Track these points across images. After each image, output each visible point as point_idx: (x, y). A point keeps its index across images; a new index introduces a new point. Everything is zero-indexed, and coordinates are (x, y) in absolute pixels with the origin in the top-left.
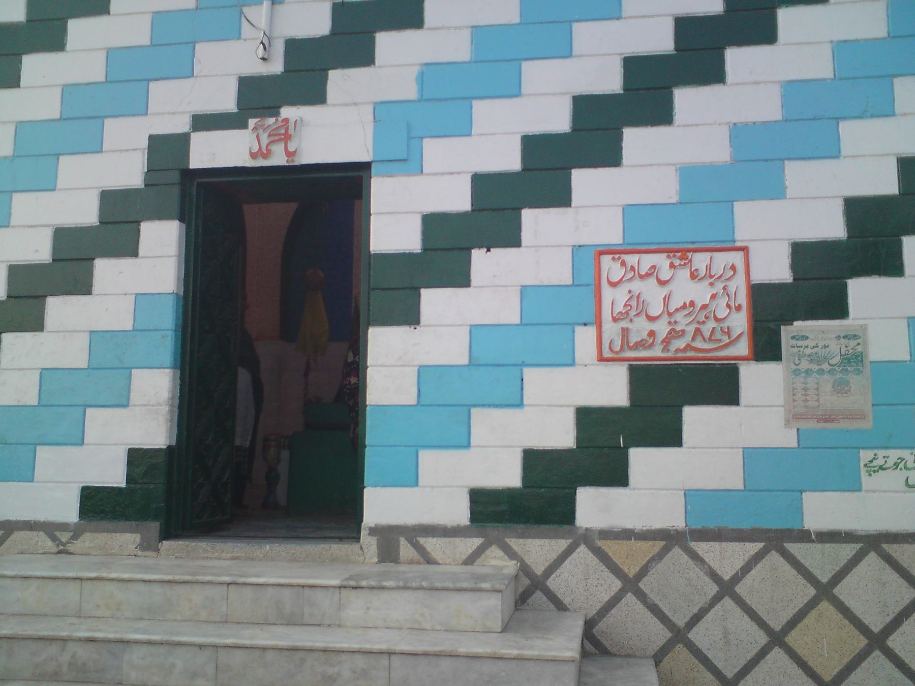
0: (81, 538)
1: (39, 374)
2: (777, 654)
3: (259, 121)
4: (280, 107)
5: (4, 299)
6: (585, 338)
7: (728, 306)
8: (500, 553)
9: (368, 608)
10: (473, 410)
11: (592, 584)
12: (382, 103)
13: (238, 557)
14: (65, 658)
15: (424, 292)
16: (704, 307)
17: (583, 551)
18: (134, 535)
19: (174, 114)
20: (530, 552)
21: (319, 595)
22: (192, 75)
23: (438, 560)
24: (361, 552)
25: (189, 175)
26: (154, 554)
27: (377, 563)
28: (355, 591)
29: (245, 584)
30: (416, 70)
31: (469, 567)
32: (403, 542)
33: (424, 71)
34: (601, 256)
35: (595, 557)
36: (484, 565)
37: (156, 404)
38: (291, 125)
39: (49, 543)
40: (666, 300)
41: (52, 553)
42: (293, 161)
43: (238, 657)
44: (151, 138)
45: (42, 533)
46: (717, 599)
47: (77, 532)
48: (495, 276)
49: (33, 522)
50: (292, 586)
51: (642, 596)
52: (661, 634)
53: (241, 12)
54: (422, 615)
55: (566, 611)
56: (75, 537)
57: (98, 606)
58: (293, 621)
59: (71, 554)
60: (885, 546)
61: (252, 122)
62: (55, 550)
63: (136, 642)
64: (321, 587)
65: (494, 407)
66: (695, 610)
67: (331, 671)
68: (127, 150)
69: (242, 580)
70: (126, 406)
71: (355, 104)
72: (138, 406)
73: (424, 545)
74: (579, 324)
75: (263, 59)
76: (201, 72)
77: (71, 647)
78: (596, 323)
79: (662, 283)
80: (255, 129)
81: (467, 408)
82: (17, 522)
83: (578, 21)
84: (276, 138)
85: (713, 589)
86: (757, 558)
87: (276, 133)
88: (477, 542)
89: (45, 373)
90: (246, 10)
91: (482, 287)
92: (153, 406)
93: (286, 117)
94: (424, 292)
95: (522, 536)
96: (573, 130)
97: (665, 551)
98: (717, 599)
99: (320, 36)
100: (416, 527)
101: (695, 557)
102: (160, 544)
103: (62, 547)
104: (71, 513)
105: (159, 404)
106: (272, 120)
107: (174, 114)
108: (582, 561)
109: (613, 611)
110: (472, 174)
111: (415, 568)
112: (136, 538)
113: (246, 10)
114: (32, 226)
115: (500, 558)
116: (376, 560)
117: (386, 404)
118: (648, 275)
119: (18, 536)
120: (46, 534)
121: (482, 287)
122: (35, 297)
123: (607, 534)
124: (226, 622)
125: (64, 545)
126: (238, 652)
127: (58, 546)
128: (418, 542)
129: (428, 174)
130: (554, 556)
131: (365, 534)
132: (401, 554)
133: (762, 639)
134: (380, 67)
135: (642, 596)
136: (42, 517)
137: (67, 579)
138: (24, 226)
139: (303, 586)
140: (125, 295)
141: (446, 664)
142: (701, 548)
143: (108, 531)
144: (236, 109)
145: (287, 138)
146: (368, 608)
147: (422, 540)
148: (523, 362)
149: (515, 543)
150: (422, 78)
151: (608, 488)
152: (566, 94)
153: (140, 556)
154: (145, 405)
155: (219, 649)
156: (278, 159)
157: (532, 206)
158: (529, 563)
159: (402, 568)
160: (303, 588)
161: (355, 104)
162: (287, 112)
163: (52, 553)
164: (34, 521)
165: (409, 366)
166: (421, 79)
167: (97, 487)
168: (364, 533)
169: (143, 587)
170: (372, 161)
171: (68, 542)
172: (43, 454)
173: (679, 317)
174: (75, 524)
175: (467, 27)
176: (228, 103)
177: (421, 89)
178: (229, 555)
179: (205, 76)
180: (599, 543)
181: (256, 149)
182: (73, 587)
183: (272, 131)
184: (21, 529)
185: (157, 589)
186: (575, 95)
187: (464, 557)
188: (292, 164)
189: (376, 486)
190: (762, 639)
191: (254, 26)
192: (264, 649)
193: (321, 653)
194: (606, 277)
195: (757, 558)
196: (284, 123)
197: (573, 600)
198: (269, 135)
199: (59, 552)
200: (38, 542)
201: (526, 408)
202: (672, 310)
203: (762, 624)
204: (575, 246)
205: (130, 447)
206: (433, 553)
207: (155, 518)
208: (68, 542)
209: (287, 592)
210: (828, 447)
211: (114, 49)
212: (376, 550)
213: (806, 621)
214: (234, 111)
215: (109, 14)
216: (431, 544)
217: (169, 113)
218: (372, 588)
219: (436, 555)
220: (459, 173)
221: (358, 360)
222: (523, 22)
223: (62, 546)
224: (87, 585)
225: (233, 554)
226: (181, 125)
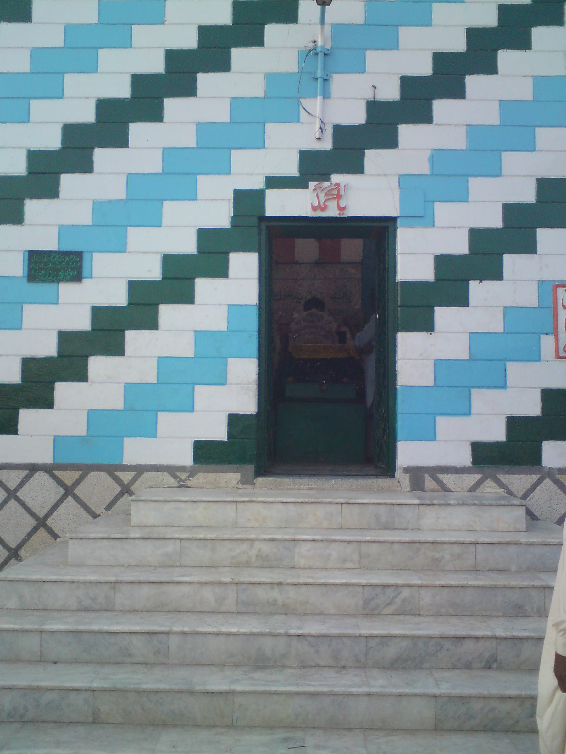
0: (196, 477)
1: (157, 360)
3: (318, 184)
4: (330, 174)
5: (126, 305)
6: (547, 342)
8: (493, 484)
9: (438, 518)
10: (473, 391)
11: (553, 503)
12: (404, 175)
13: (312, 488)
14: (253, 552)
15: (437, 309)
17: (547, 482)
18: (236, 474)
19: (251, 174)
20: (512, 484)
21: (405, 509)
22: (264, 147)
23: (451, 489)
24: (398, 484)
25: (263, 219)
26: (251, 487)
27: (410, 491)
28: (429, 507)
29: (354, 503)
30: (428, 153)
31: (473, 494)
32: (427, 478)
33: (434, 154)
34: (558, 288)
35: (555, 486)
36: (483, 492)
37: (247, 383)
38: (342, 188)
39: (172, 480)
41: (175, 487)
42: (343, 214)
43: (374, 548)
44: (236, 192)
47: (192, 473)
48: (485, 300)
49: (158, 466)
50: (386, 504)
53: (299, 102)
54: (474, 522)
55: (537, 520)
56: (191, 476)
57: (249, 520)
58: (388, 527)
59: (189, 487)
61: (312, 184)
62: (177, 485)
63: (304, 540)
64: (406, 504)
65: (487, 388)
67: (437, 555)
68: (216, 200)
69: (352, 501)
70: (224, 384)
71: (385, 175)
72: (233, 384)
73: (442, 480)
74: (543, 334)
75: (319, 139)
76: (270, 145)
77: (257, 545)
78: (554, 333)
80: (315, 189)
81: (468, 389)
82: (146, 466)
83: (539, 126)
84: (331, 197)
87: (330, 193)
88: (478, 477)
89: (161, 360)
90: (302, 101)
91: (477, 307)
92: (245, 384)
93: (337, 181)
94: (437, 309)
95: (508, 473)
96: (537, 202)
99: (358, 124)
100: (436, 467)
102: (255, 480)
103: (182, 483)
104: (187, 459)
105: (249, 383)
106: (326, 184)
107: (251, 174)
108: (547, 488)
110: (469, 228)
111: (436, 494)
112: (238, 476)
113: (302, 101)
114: (144, 253)
117: (412, 385)
119: (147, 475)
120: (169, 474)
121: (477, 307)
122: (150, 305)
124: (341, 528)
125: (183, 481)
126: (374, 545)
127: (179, 482)
128: (437, 477)
129: (437, 227)
130: (529, 485)
131: (401, 472)
132: (426, 485)
134: (402, 150)
137: (227, 502)
138: (138, 252)
139: (394, 504)
140: (220, 305)
141: (512, 549)
143: (217, 471)
144: (298, 173)
145: (339, 197)
146: (438, 518)
147: (440, 476)
148: (506, 358)
149: (503, 478)
150: (433, 159)
151: (563, 441)
152: (532, 176)
153: (241, 488)
154: (239, 384)
155: (362, 543)
156: (332, 212)
157: (510, 253)
158: (513, 491)
159: (427, 494)
160: (394, 505)
161: (385, 175)
162: (336, 178)
163: (175, 487)
164: (159, 465)
165: (427, 359)
166: (432, 159)
167: (206, 441)
169: (281, 506)
170: (399, 217)
171: (186, 480)
172: (162, 417)
174: (191, 466)
175: (464, 125)
177: (432, 167)
178: (306, 487)
179: (273, 148)
180: (558, 477)
181: (316, 204)
182: (233, 507)
183: (328, 191)
184: (150, 471)
185: (291, 507)
186: (538, 177)
187: (469, 487)
188: (342, 216)
189: (407, 441)
191: (310, 114)
192: (392, 543)
193: (431, 544)
194: (561, 302)
196: (336, 187)
197: (542, 513)
198: (326, 195)
199: (179, 487)
200: (163, 480)
201: (509, 389)
204: (539, 281)
205: (229, 413)
206: (447, 484)
207: (250, 462)
208: (186, 480)
209: (383, 508)
210: (460, 413)
211: (203, 123)
212: (409, 483)
214: (296, 175)
215: (196, 96)
216: (446, 478)
217: (247, 174)
219: (450, 485)
220: (460, 227)
222: (501, 124)
223: (182, 482)
224: (241, 506)
225: (309, 486)
226: (258, 184)
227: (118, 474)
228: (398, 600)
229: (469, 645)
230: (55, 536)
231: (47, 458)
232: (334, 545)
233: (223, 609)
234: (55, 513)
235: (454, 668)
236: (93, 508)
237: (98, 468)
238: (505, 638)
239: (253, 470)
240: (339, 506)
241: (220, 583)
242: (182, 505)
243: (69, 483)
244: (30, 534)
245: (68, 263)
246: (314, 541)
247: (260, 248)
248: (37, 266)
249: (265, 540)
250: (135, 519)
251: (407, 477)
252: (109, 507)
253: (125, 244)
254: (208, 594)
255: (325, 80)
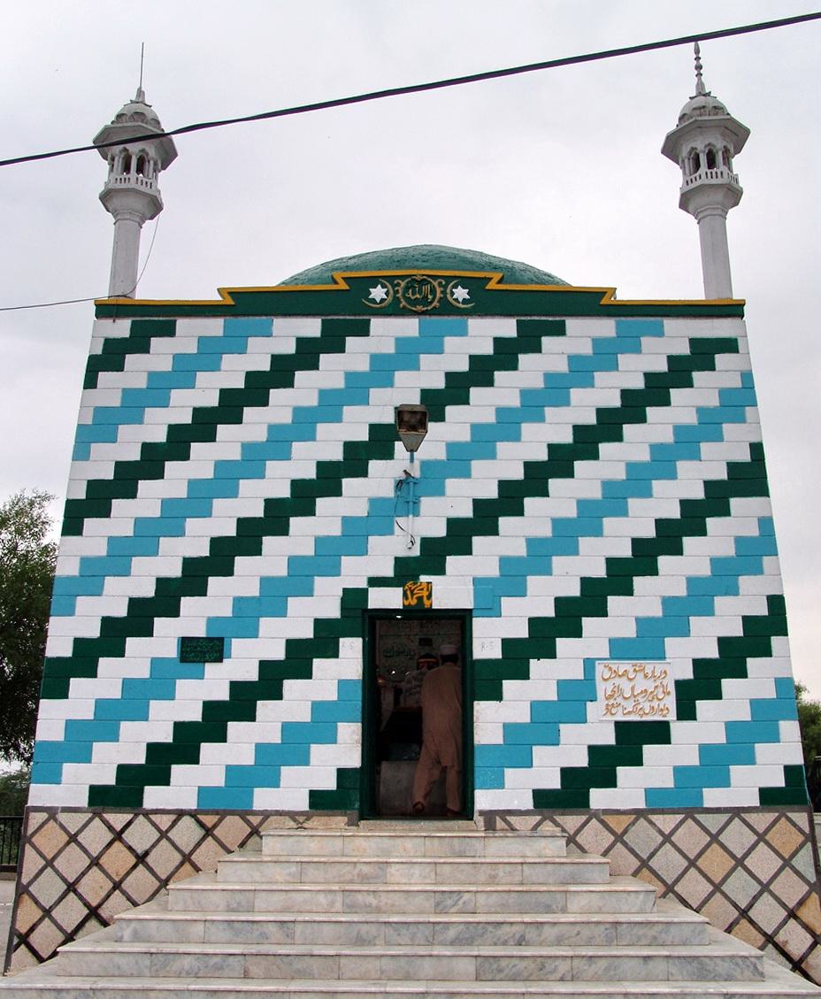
2: (693, 871)
7: (664, 692)
14: (356, 871)
16: (652, 692)
21: (474, 841)
39: (292, 824)
40: (633, 688)
45: (287, 817)
46: (662, 844)
51: (625, 844)
52: (637, 863)
60: (742, 815)
66: (652, 850)
79: (630, 680)
85: (660, 839)
86: (682, 822)
88: (539, 818)
95: (563, 814)
97: (636, 820)
98: (662, 844)
101: (651, 822)
104: (303, 804)
109: (611, 852)
115: (551, 826)
116: (483, 829)
118: (623, 675)
123: (607, 812)
133: (686, 864)
135: (625, 844)
136: (286, 808)
141: (549, 867)
142: (654, 818)
143: (328, 815)
147: (508, 818)
149: (558, 818)
168: (476, 816)
173: (639, 698)
176: (389, 572)
185: (386, 840)
190: (686, 864)
195: (682, 822)
202: (636, 694)
203: (685, 856)
213: (706, 853)
216: (511, 819)
218: (501, 837)
221: (59, 644)
226: (363, 584)
227: (249, 817)
228: (461, 902)
229: (506, 928)
230: (197, 869)
231: (193, 805)
232: (416, 866)
233: (333, 910)
234: (198, 850)
235: (495, 944)
236: (229, 846)
237: (233, 813)
238: (530, 923)
239: (357, 814)
240: (423, 839)
241: (330, 891)
242: (302, 839)
243: (209, 825)
244: (178, 868)
245: (212, 647)
246: (402, 863)
247: (363, 631)
248: (188, 649)
249: (365, 863)
250: (265, 850)
251: (481, 819)
252: (242, 845)
253: (257, 630)
254: (322, 899)
255: (415, 503)
